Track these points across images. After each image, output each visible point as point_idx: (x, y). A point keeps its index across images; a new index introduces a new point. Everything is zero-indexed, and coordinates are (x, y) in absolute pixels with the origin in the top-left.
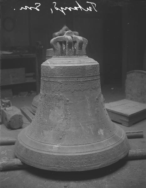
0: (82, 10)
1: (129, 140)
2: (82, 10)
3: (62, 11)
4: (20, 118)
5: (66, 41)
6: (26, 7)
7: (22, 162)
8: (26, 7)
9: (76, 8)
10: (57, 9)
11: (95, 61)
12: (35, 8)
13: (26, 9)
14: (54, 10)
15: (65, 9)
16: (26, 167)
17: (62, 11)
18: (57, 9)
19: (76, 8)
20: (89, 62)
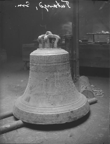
0: (24, 7)
1: (91, 105)
2: (24, 7)
3: (46, 8)
4: (14, 103)
5: (13, 114)
6: (48, 5)
7: (23, 122)
8: (48, 5)
9: (55, 6)
10: (43, 7)
11: (66, 51)
12: (26, 6)
13: (49, 7)
14: (39, 8)
15: (47, 7)
16: (27, 125)
17: (46, 8)
18: (43, 7)
19: (55, 6)
20: (62, 52)
